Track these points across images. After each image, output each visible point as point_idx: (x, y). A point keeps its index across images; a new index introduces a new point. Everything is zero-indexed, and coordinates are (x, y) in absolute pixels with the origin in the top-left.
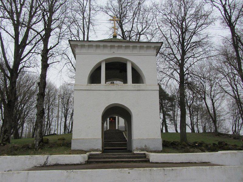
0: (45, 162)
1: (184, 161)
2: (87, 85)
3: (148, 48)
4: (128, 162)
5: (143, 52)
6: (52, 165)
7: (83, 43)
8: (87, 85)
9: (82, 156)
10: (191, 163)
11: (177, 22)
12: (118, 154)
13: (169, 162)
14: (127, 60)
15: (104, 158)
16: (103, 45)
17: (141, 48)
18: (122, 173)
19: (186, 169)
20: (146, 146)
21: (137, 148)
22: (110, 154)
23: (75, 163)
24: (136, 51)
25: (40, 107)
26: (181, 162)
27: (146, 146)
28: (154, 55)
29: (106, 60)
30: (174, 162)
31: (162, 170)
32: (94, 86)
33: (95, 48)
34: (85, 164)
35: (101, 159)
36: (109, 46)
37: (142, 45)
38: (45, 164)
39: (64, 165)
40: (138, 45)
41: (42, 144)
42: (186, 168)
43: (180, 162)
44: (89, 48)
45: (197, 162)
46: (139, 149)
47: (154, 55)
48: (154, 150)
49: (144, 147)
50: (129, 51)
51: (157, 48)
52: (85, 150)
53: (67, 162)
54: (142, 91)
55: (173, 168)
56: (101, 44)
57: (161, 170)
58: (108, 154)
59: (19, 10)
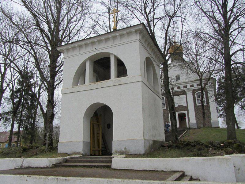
0: (22, 164)
1: (147, 169)
2: (72, 87)
3: (129, 34)
4: (90, 167)
5: (125, 40)
6: (25, 168)
7: (114, 34)
8: (72, 87)
9: (48, 160)
10: (157, 171)
11: (79, 13)
12: (95, 158)
13: (129, 169)
14: (110, 54)
15: (84, 162)
16: (119, 34)
17: (122, 36)
18: (21, 180)
19: (79, 181)
20: (125, 148)
21: (116, 151)
22: (88, 158)
23: (42, 166)
24: (117, 42)
25: (49, 114)
26: (144, 169)
27: (125, 148)
28: (136, 40)
29: (90, 59)
30: (135, 168)
31: (56, 180)
32: (80, 87)
33: (135, 34)
34: (52, 167)
35: (76, 162)
36: (89, 43)
37: (121, 33)
38: (21, 166)
39: (34, 168)
40: (117, 34)
41: (51, 147)
42: (80, 179)
43: (142, 169)
44: (99, 43)
45: (165, 170)
46: (119, 152)
47: (136, 40)
48: (135, 153)
49: (123, 150)
50: (110, 43)
51: (139, 32)
52: (69, 153)
53: (37, 166)
54: (122, 85)
55: (67, 178)
56: (76, 44)
57: (54, 179)
58: (86, 158)
59: (67, 15)
